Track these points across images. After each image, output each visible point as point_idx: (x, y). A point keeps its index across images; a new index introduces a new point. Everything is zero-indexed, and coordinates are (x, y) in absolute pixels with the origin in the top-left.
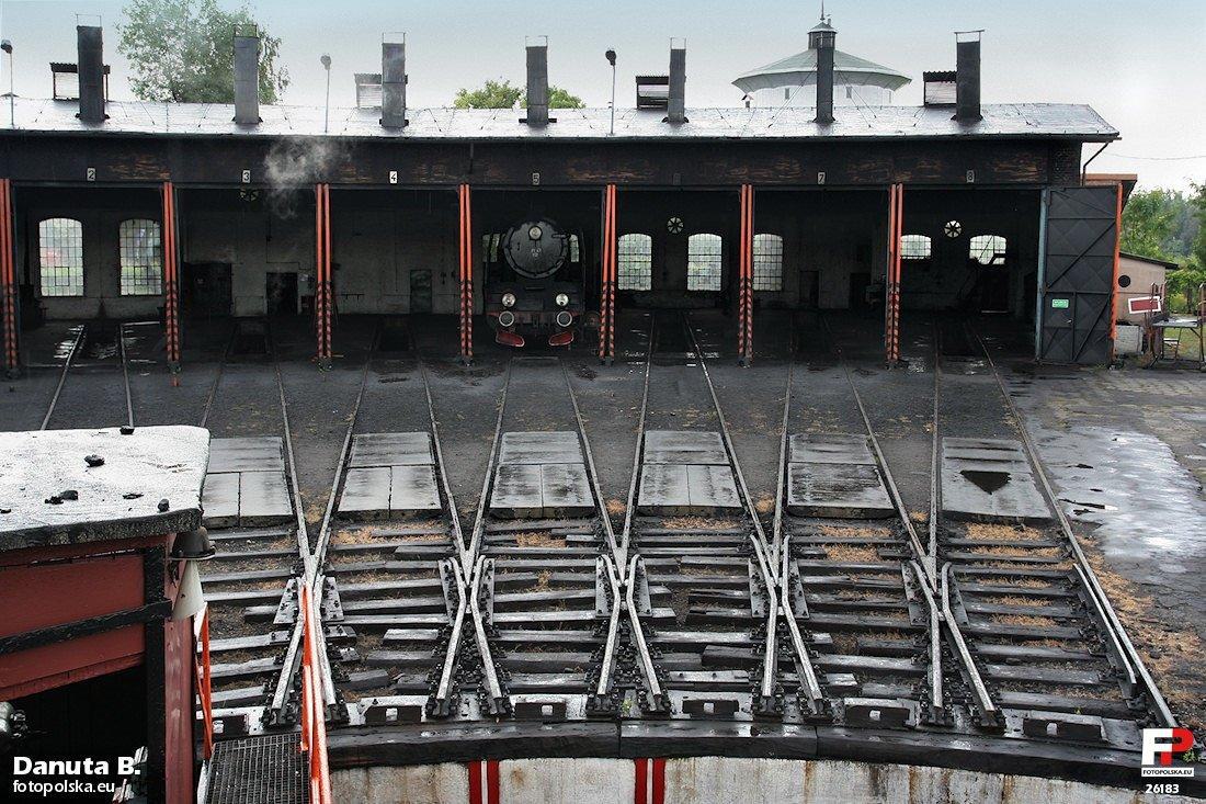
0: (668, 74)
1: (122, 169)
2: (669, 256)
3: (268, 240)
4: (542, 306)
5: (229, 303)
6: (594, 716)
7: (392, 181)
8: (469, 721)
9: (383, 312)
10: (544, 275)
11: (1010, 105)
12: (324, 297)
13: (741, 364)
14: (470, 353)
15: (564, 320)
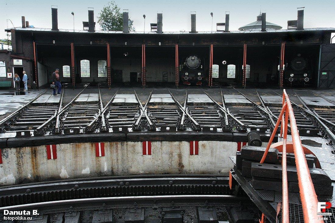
0: (225, 22)
1: (98, 42)
2: (223, 70)
3: (130, 65)
4: (194, 75)
5: (122, 79)
6: (225, 131)
7: (160, 45)
8: (190, 131)
9: (156, 82)
10: (195, 68)
11: (311, 24)
12: (144, 77)
13: (243, 88)
14: (178, 85)
15: (200, 79)
